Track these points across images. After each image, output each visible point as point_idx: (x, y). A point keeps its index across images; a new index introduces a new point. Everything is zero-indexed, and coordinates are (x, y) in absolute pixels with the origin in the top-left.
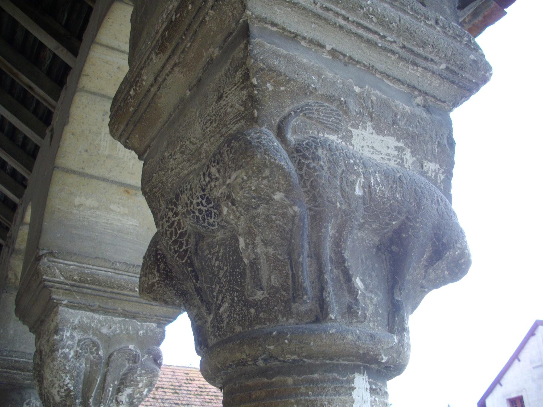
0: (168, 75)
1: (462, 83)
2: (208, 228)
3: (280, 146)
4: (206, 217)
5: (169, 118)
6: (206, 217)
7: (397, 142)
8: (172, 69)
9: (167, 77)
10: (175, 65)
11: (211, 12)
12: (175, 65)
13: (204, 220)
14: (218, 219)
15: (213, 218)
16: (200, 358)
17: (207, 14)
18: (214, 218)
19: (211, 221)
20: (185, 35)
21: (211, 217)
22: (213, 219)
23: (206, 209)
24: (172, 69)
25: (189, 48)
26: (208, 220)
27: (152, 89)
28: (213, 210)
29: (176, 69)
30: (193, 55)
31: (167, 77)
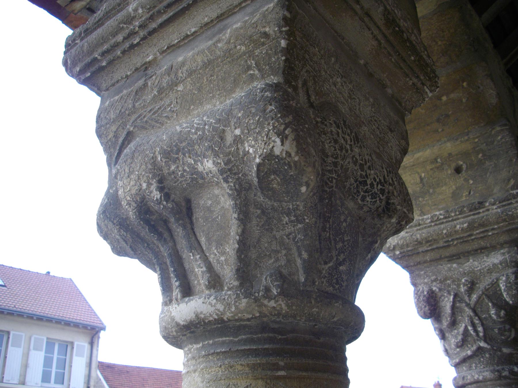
0: (372, 33)
1: (133, 217)
2: (358, 196)
3: (208, 107)
4: (370, 193)
5: (339, 36)
6: (370, 193)
7: (326, 265)
8: (377, 39)
9: (370, 32)
10: (380, 44)
11: (411, 83)
12: (380, 44)
13: (366, 191)
14: (371, 204)
15: (371, 200)
16: (357, 303)
17: (411, 79)
18: (371, 202)
19: (368, 199)
20: (399, 55)
21: (372, 199)
22: (369, 200)
23: (376, 191)
24: (377, 39)
25: (391, 59)
26: (368, 196)
27: (358, 6)
28: (378, 199)
29: (375, 43)
30: (384, 61)
31: (370, 32)
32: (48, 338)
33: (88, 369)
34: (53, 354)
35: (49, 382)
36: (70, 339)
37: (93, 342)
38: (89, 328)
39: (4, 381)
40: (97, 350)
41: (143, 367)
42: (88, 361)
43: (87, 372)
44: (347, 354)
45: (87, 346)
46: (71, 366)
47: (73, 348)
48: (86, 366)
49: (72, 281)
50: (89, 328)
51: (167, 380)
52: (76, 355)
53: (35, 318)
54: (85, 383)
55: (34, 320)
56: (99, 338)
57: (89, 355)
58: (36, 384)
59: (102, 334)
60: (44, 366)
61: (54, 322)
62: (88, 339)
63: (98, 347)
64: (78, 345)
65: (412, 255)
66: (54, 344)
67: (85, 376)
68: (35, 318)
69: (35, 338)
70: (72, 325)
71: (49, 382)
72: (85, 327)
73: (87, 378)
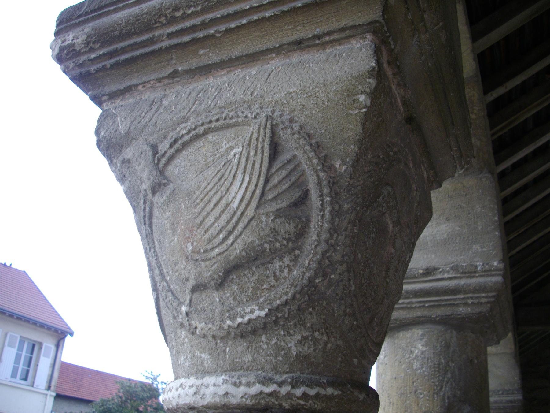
16: (370, 385)
32: (21, 336)
33: (51, 369)
34: (22, 351)
35: (16, 378)
36: (39, 340)
37: (59, 345)
38: (60, 332)
39: (35, 386)
40: (61, 353)
41: (88, 369)
42: (53, 362)
43: (50, 373)
44: (15, 267)
45: (53, 348)
46: (38, 365)
47: (41, 348)
48: (50, 367)
49: (26, 274)
50: (60, 332)
51: (72, 375)
52: (44, 356)
53: (15, 317)
54: (47, 382)
55: (14, 318)
56: (64, 341)
57: (54, 357)
58: (6, 378)
59: (68, 338)
60: (15, 363)
61: (31, 322)
62: (55, 341)
63: (62, 349)
64: (46, 346)
65: (206, 133)
66: (24, 342)
67: (48, 376)
68: (15, 317)
69: (11, 335)
70: (46, 327)
71: (16, 378)
72: (56, 331)
73: (49, 378)
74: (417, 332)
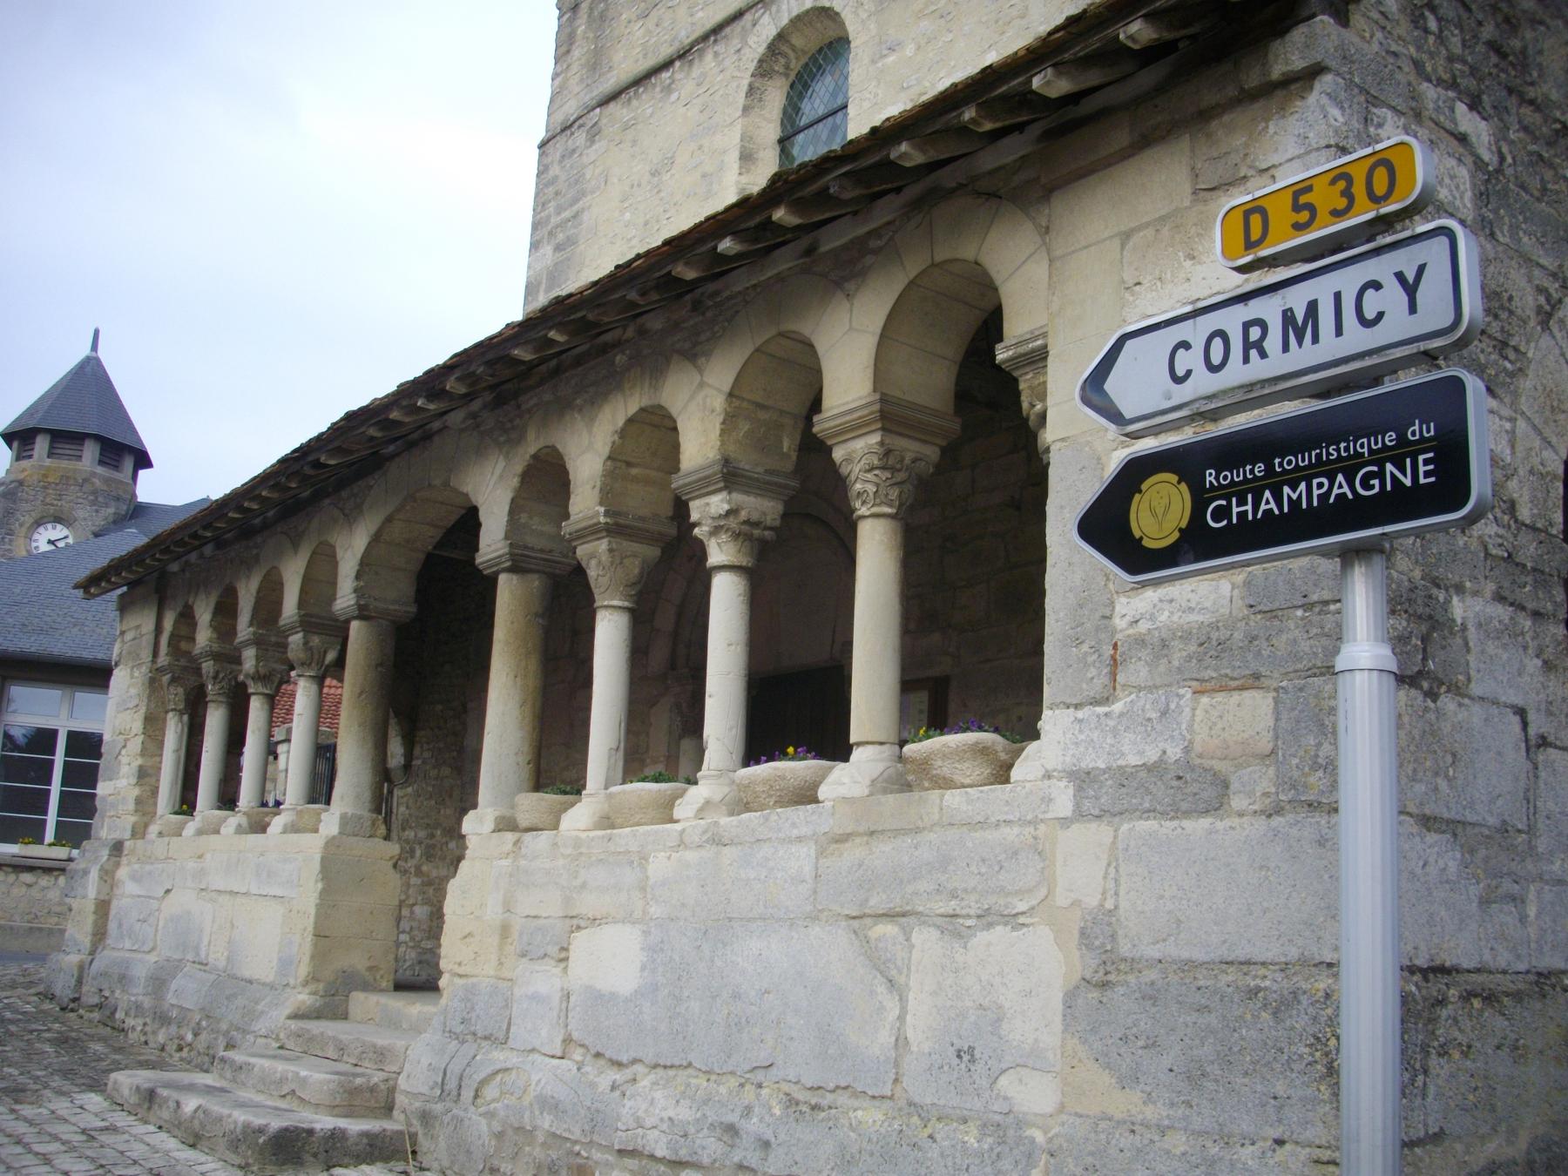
74: (536, 576)
